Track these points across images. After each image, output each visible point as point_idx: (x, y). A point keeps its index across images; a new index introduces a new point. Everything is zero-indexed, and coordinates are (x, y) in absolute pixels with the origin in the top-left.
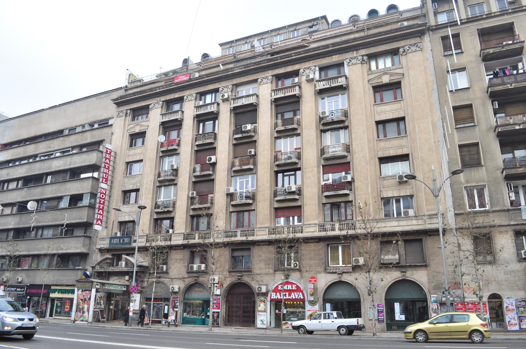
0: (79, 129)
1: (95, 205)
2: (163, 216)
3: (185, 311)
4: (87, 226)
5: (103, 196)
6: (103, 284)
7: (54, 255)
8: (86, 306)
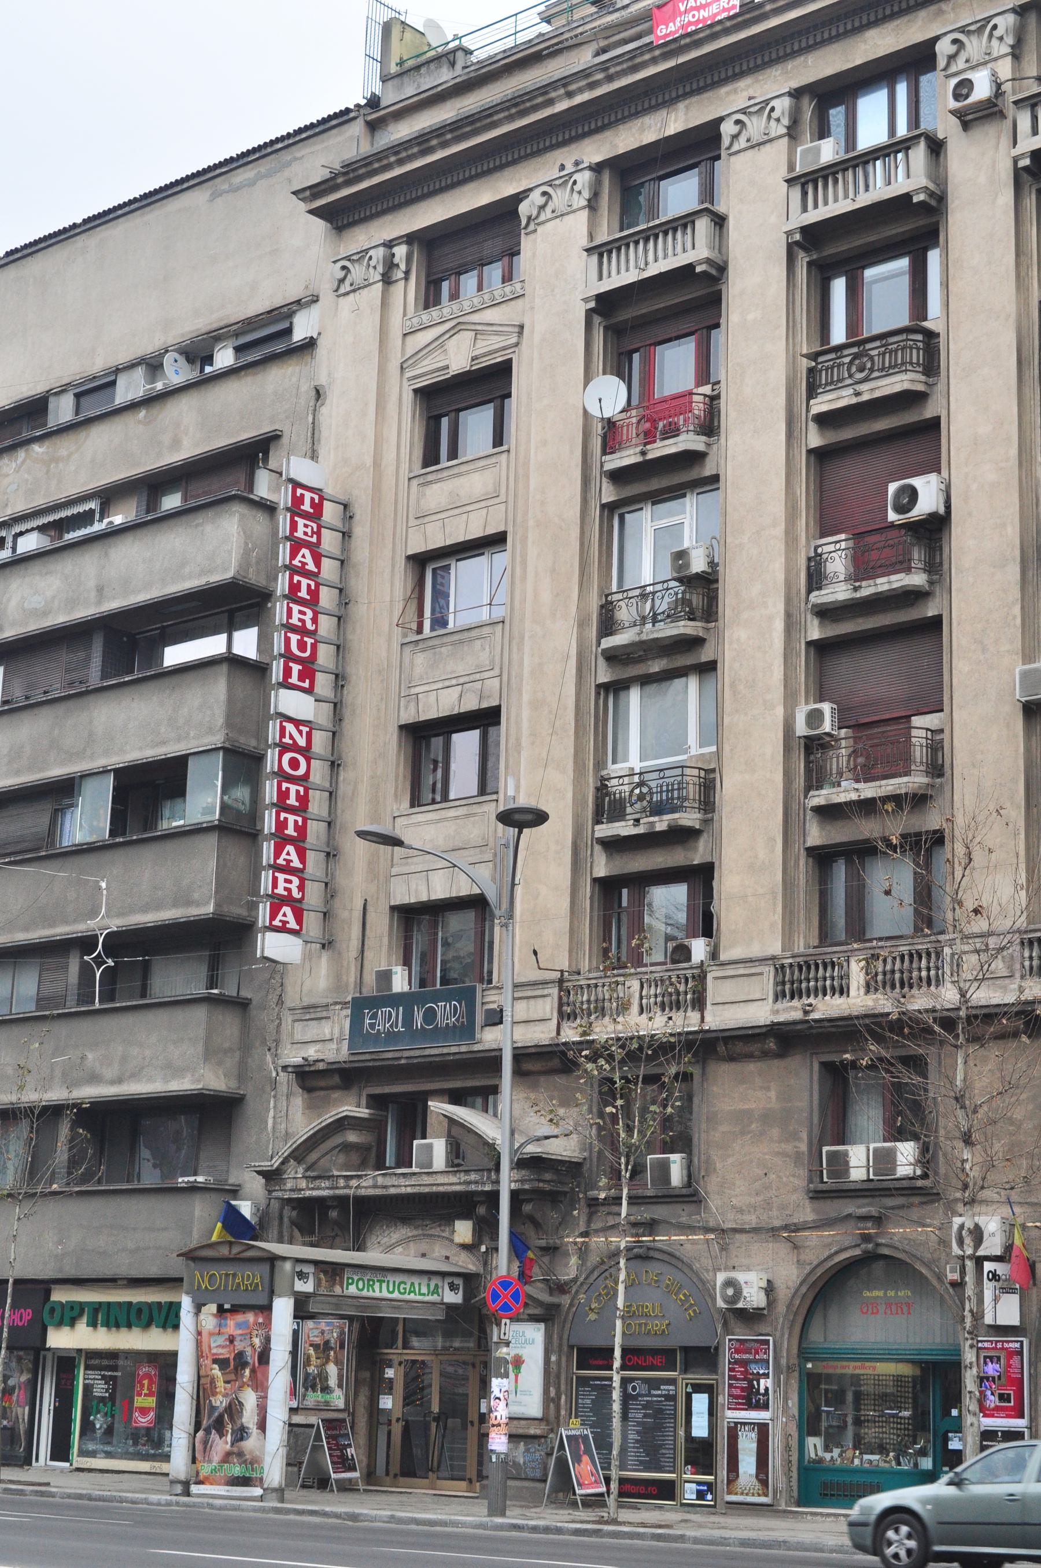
0: (131, 388)
1: (254, 815)
2: (649, 859)
3: (810, 1424)
4: (221, 939)
5: (294, 764)
6: (333, 1271)
7: (53, 1112)
8: (250, 1399)
